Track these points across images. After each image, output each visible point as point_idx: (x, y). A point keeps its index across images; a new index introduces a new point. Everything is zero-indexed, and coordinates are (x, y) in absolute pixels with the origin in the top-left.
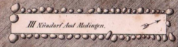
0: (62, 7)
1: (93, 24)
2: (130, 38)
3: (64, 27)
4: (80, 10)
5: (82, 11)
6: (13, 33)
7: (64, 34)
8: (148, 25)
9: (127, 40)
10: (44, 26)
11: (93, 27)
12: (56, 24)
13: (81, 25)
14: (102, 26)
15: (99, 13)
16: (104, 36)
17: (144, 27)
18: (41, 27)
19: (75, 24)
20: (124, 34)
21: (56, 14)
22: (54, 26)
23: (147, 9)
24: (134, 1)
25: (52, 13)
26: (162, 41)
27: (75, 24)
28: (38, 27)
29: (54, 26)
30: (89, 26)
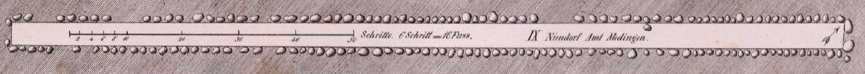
0: (463, 11)
1: (630, 36)
2: (743, 53)
3: (546, 40)
4: (211, 18)
5: (75, 18)
6: (843, 45)
7: (749, 49)
8: (829, 37)
9: (450, 55)
10: (556, 38)
11: (629, 40)
12: (573, 35)
13: (612, 37)
14: (558, 39)
15: (808, 22)
16: (335, 50)
17: (825, 42)
18: (552, 39)
19: (603, 35)
20: (649, 49)
21: (749, 24)
22: (568, 38)
23: (231, 15)
24: (502, 1)
25: (74, 22)
26: (315, 55)
27: (603, 35)
28: (546, 40)
29: (568, 38)
30: (623, 37)
